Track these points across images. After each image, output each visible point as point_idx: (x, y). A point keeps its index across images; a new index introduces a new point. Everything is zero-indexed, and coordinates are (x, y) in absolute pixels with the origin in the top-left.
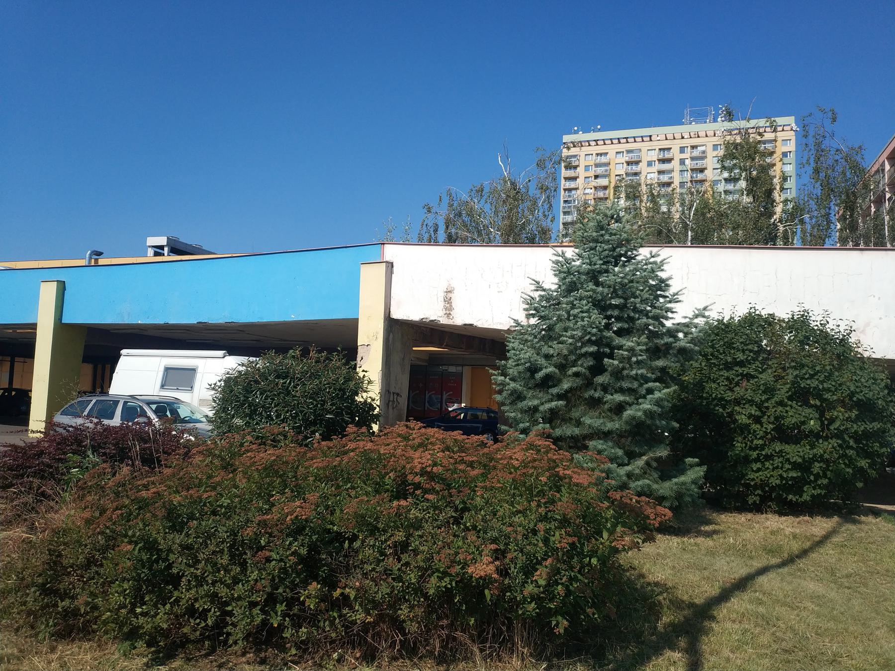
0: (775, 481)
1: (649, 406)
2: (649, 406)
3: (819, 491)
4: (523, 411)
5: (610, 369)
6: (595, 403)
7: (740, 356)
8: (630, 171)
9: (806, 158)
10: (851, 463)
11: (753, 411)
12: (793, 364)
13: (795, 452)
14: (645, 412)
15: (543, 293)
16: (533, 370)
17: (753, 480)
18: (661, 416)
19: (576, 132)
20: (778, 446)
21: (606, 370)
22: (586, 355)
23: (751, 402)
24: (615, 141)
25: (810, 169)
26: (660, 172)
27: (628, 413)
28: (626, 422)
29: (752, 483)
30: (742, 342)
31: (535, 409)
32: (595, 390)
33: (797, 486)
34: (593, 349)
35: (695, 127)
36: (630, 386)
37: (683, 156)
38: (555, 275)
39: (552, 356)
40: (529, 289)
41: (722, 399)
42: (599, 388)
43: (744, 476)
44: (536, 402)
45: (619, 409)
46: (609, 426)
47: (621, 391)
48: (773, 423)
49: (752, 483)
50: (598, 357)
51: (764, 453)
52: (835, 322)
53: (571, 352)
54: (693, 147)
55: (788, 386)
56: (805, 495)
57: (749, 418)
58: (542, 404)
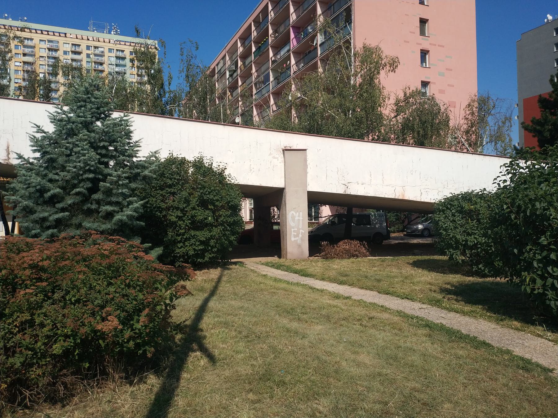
0: (191, 253)
1: (131, 213)
2: (131, 213)
3: (213, 255)
4: (35, 222)
5: (102, 189)
6: (89, 213)
7: (170, 182)
8: (50, 55)
9: (182, 67)
10: (227, 239)
11: (179, 214)
12: (200, 186)
13: (202, 235)
14: (127, 216)
15: (44, 134)
16: (42, 191)
17: (179, 253)
18: (138, 219)
19: (6, 18)
20: (193, 233)
21: (99, 190)
22: (88, 179)
23: (177, 209)
24: (39, 32)
25: (184, 75)
26: (73, 60)
27: (118, 217)
28: (115, 224)
29: (178, 255)
30: (172, 173)
31: (44, 219)
32: (91, 204)
33: (200, 254)
34: (91, 176)
35: (96, 34)
36: (117, 200)
37: (89, 52)
38: (51, 122)
39: (58, 181)
40: (32, 131)
41: (160, 207)
42: (94, 202)
43: (173, 251)
44: (46, 214)
45: (109, 216)
46: (104, 227)
47: (110, 203)
48: (189, 220)
49: (178, 255)
50: (95, 182)
51: (185, 237)
52: (217, 164)
53: (73, 178)
54: (96, 47)
55: (197, 199)
56: (206, 258)
57: (176, 218)
58: (50, 215)
